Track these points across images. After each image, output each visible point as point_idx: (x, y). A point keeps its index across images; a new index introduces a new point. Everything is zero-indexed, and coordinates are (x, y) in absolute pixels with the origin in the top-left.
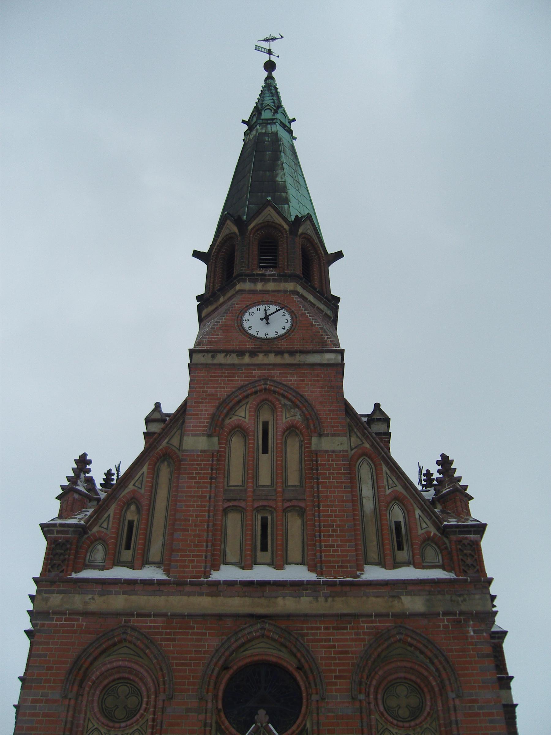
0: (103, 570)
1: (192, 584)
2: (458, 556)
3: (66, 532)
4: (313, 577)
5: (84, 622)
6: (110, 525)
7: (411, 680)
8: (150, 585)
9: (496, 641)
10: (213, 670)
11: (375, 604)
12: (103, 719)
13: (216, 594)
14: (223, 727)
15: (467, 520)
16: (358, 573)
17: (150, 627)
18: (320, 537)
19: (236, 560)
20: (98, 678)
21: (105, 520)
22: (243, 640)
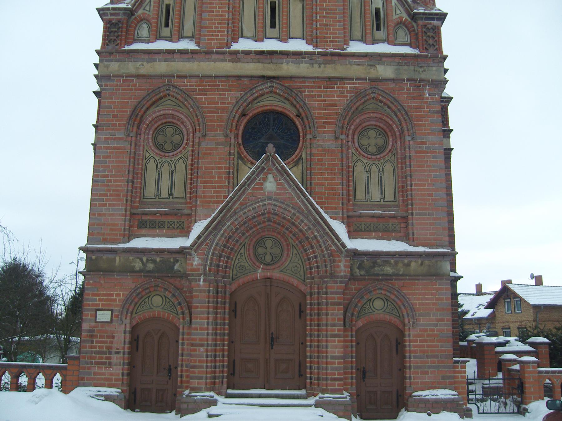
0: (148, 43)
1: (217, 53)
2: (422, 37)
3: (118, 14)
4: (310, 48)
5: (137, 82)
6: (152, 8)
7: (379, 127)
8: (185, 54)
9: (443, 104)
10: (235, 116)
11: (356, 70)
12: (156, 151)
13: (237, 61)
15: (432, 9)
16: (345, 46)
17: (187, 85)
18: (316, 18)
19: (251, 34)
20: (150, 122)
21: (147, 5)
22: (256, 95)
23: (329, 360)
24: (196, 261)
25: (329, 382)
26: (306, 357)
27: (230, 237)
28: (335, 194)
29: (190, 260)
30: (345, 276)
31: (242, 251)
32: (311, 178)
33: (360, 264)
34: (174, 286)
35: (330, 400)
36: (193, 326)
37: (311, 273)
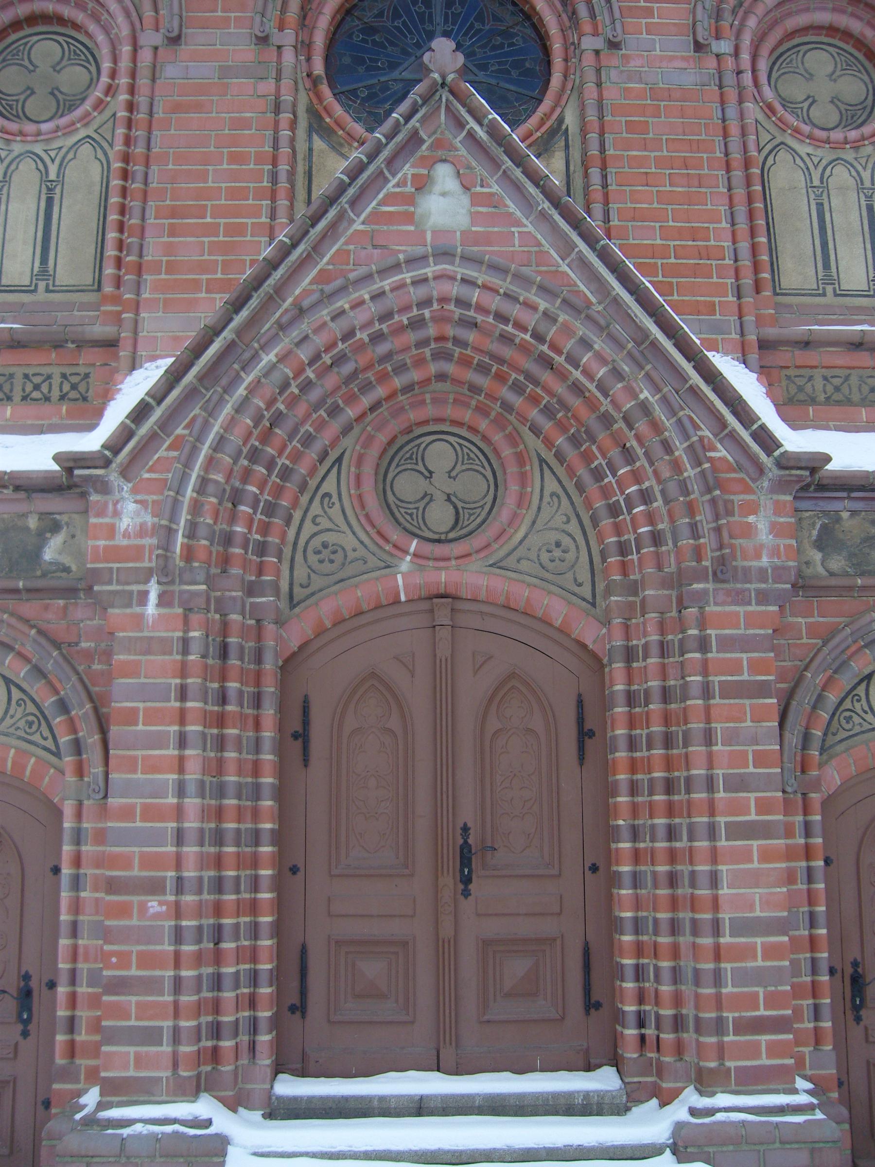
14: (328, 120)
23: (726, 940)
24: (129, 514)
25: (729, 1038)
26: (614, 925)
27: (277, 419)
28: (705, 253)
29: (101, 514)
30: (775, 568)
31: (330, 486)
32: (606, 196)
33: (824, 527)
34: (40, 632)
35: (743, 1123)
36: (113, 801)
37: (624, 569)
